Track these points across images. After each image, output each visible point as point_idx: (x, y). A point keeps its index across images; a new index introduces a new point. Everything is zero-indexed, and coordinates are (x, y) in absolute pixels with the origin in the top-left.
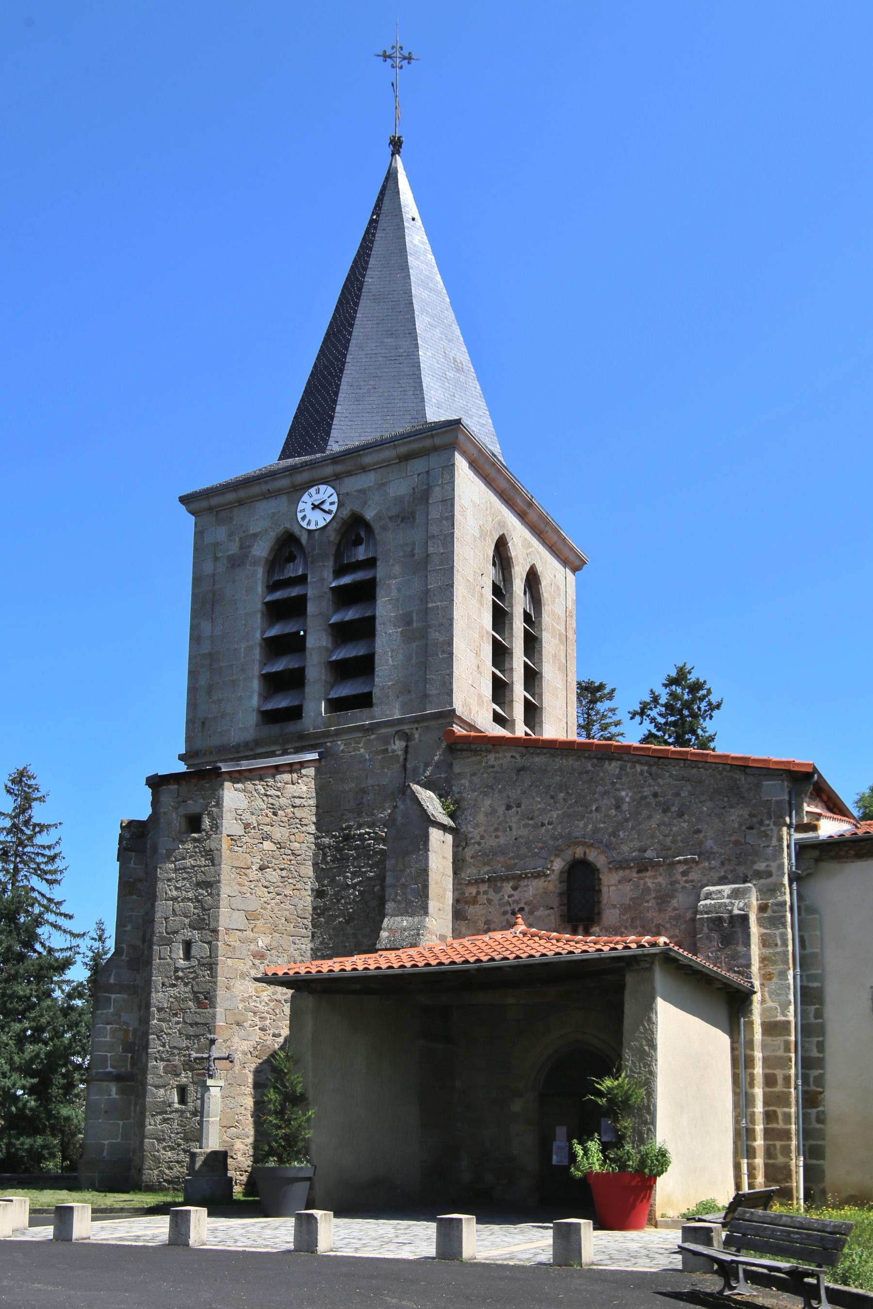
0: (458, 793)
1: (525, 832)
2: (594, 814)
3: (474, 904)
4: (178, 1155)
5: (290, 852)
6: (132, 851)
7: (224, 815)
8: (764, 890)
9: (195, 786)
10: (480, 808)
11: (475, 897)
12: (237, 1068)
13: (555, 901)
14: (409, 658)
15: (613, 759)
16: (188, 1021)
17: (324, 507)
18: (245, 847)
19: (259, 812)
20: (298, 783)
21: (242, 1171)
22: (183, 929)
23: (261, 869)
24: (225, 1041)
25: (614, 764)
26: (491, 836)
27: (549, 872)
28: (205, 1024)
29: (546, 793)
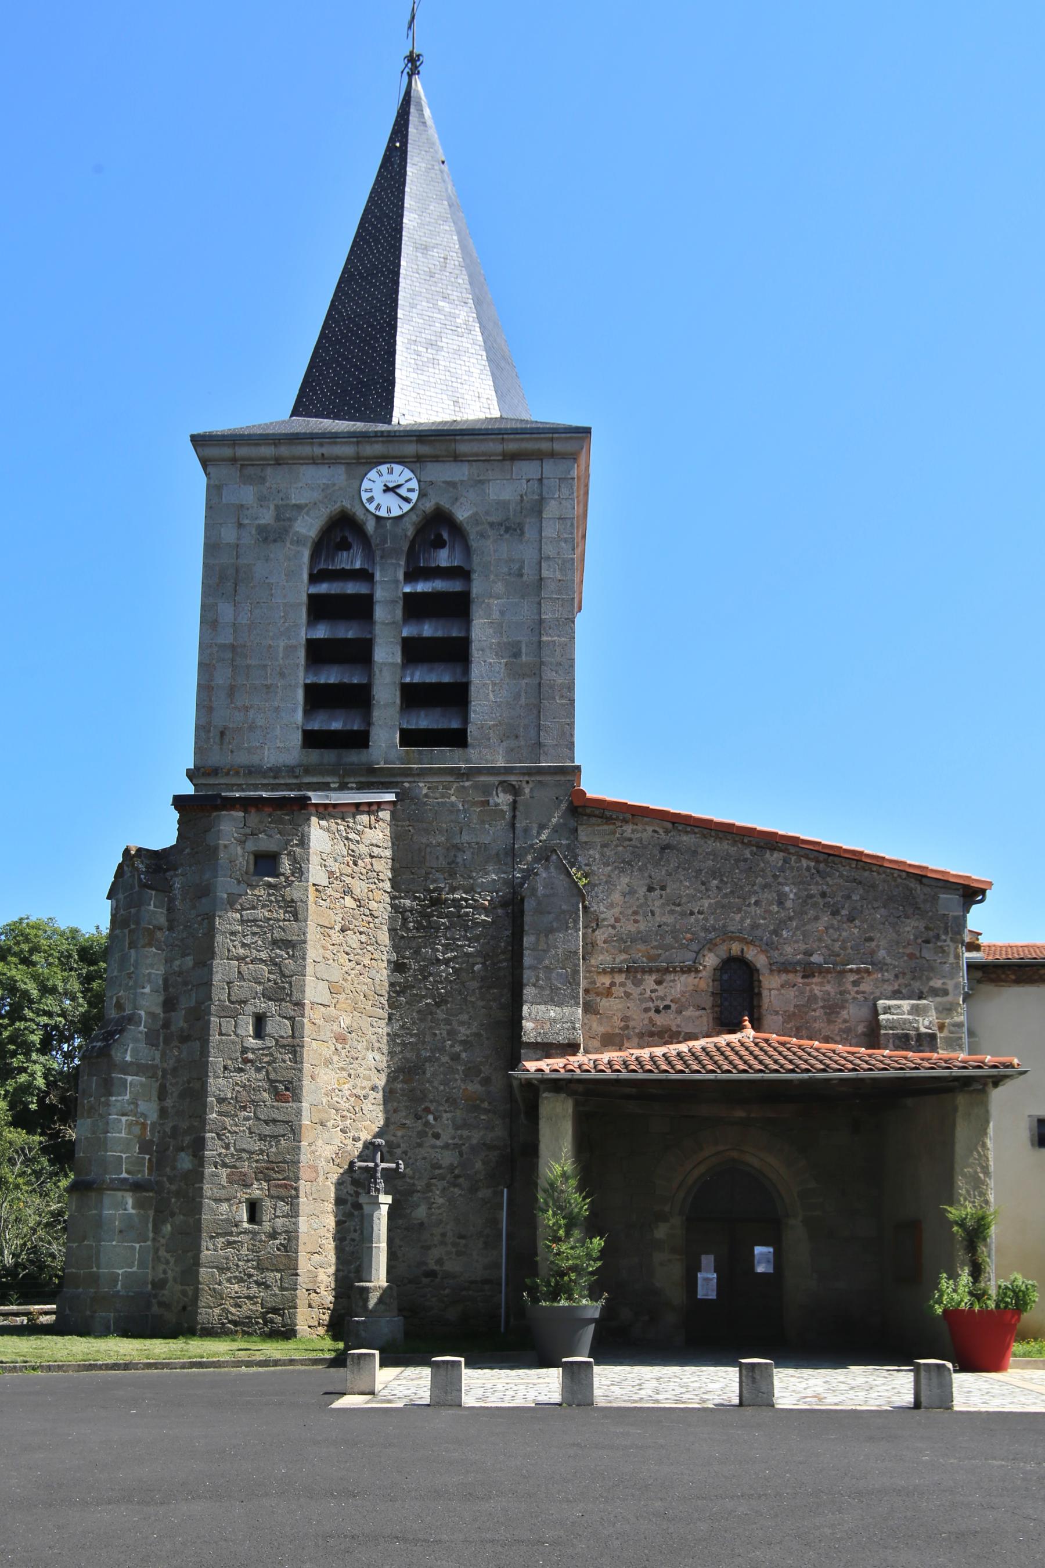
0: (586, 865)
1: (669, 919)
2: (753, 908)
3: (607, 996)
4: (248, 1288)
5: (368, 912)
6: (153, 889)
7: (311, 859)
8: (940, 1009)
9: (270, 815)
10: (615, 886)
11: (609, 988)
12: (321, 1179)
13: (708, 1001)
14: (517, 696)
15: (775, 849)
16: (262, 1117)
17: (400, 491)
18: (328, 901)
19: (340, 859)
20: (375, 828)
21: (324, 1308)
22: (255, 999)
23: (343, 930)
24: (310, 1144)
25: (776, 854)
26: (628, 920)
27: (701, 968)
28: (287, 1122)
29: (696, 877)
